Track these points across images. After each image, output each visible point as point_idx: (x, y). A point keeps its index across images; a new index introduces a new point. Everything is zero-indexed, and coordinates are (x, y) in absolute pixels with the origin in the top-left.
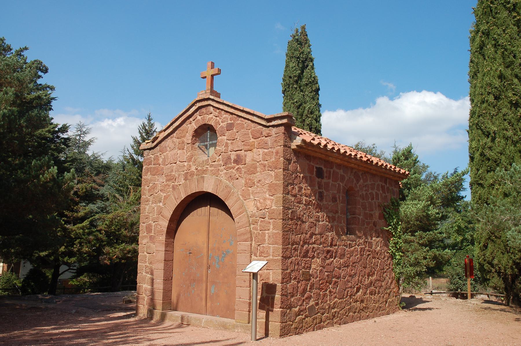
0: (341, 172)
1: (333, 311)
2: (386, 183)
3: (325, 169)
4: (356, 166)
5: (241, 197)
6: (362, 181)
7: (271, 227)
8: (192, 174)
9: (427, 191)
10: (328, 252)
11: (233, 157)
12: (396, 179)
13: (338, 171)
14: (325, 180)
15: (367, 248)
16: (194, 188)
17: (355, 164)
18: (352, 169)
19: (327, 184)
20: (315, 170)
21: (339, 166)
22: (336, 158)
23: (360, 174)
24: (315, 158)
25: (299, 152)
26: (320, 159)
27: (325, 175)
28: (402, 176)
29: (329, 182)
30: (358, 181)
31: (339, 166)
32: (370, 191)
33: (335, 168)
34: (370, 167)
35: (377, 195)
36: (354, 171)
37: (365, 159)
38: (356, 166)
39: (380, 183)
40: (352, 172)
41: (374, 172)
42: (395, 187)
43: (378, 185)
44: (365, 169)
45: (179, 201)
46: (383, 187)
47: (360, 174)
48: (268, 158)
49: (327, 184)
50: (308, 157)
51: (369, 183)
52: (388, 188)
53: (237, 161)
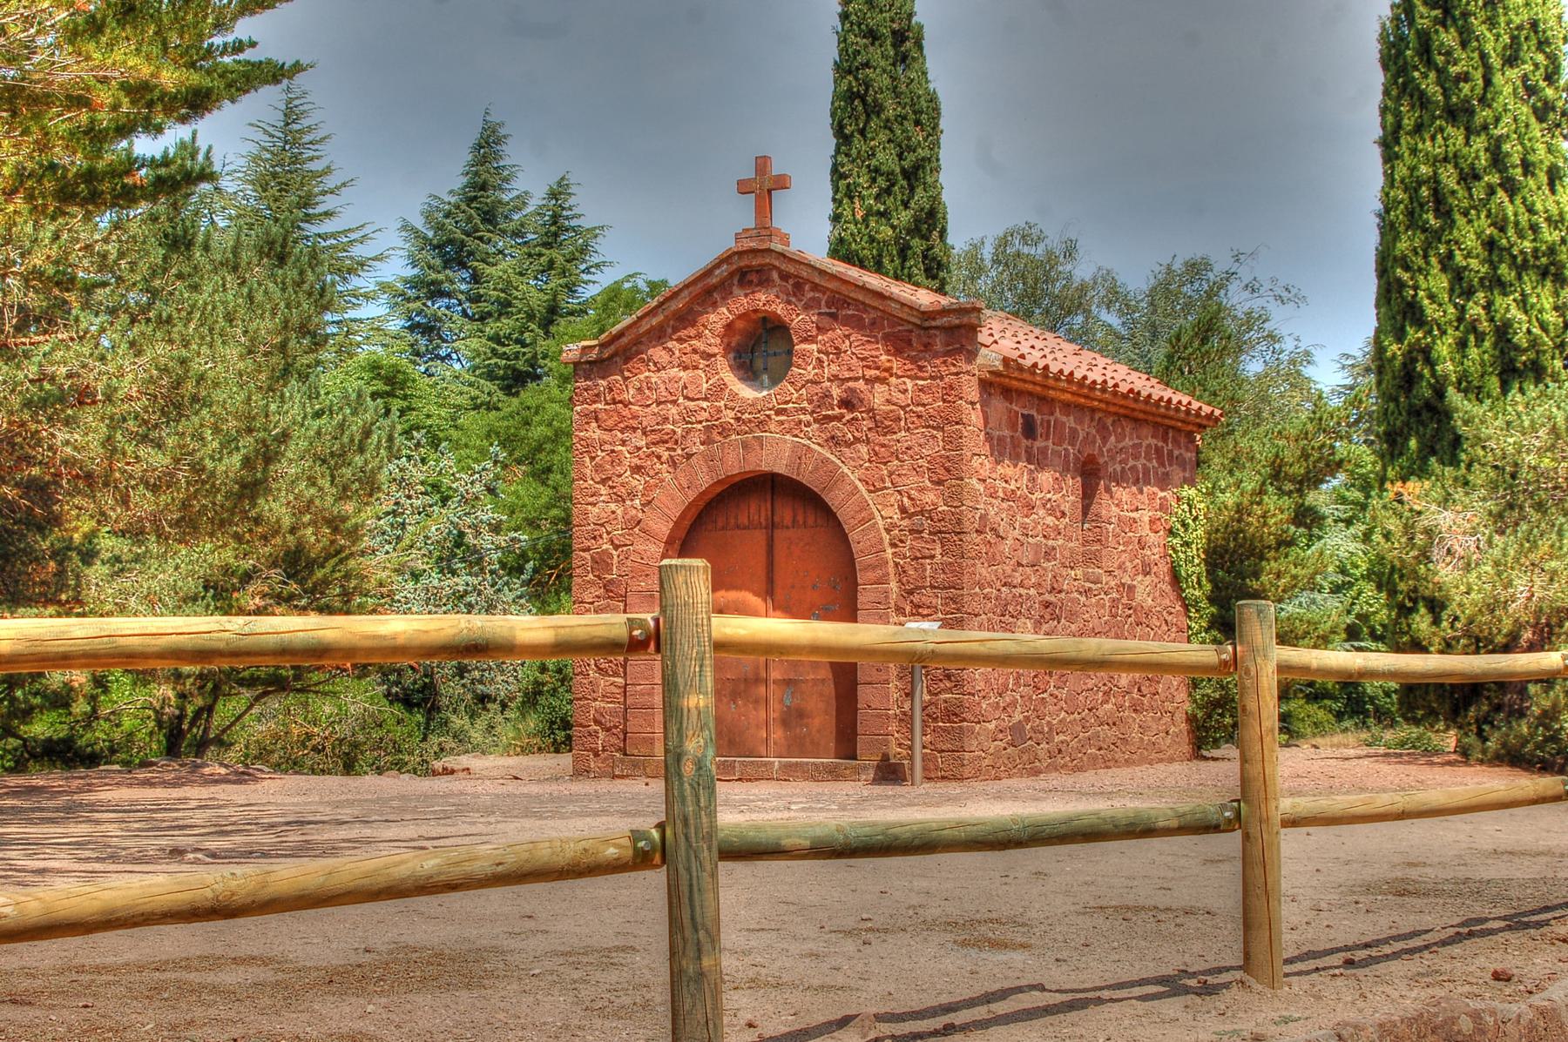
0: (1070, 422)
1: (1057, 739)
2: (1165, 441)
3: (1038, 418)
4: (1103, 406)
5: (859, 485)
6: (1113, 438)
7: (939, 551)
8: (725, 431)
9: (1258, 446)
10: (1047, 605)
11: (836, 392)
12: (1190, 428)
13: (1064, 419)
14: (1039, 443)
15: (1125, 600)
16: (734, 463)
17: (1100, 401)
18: (1093, 410)
19: (1043, 451)
20: (1020, 421)
21: (1067, 407)
22: (1063, 390)
23: (1109, 421)
24: (1020, 393)
25: (991, 384)
26: (1030, 394)
27: (1040, 430)
28: (1205, 422)
29: (1046, 448)
30: (1105, 440)
31: (1067, 407)
32: (1131, 463)
33: (1057, 413)
34: (1133, 405)
35: (1146, 471)
36: (1097, 416)
37: (1123, 388)
38: (1103, 406)
39: (1153, 442)
40: (1092, 420)
41: (1141, 416)
42: (1187, 449)
43: (1149, 446)
44: (1122, 411)
45: (692, 495)
46: (1158, 451)
47: (1109, 421)
48: (925, 398)
49: (1043, 451)
50: (1007, 393)
51: (1128, 442)
52: (1170, 453)
53: (846, 403)
